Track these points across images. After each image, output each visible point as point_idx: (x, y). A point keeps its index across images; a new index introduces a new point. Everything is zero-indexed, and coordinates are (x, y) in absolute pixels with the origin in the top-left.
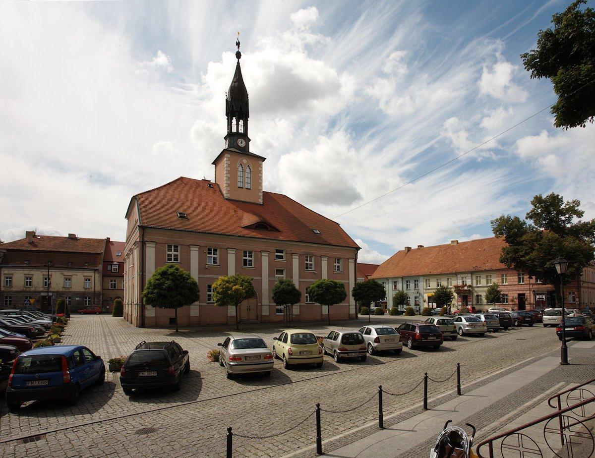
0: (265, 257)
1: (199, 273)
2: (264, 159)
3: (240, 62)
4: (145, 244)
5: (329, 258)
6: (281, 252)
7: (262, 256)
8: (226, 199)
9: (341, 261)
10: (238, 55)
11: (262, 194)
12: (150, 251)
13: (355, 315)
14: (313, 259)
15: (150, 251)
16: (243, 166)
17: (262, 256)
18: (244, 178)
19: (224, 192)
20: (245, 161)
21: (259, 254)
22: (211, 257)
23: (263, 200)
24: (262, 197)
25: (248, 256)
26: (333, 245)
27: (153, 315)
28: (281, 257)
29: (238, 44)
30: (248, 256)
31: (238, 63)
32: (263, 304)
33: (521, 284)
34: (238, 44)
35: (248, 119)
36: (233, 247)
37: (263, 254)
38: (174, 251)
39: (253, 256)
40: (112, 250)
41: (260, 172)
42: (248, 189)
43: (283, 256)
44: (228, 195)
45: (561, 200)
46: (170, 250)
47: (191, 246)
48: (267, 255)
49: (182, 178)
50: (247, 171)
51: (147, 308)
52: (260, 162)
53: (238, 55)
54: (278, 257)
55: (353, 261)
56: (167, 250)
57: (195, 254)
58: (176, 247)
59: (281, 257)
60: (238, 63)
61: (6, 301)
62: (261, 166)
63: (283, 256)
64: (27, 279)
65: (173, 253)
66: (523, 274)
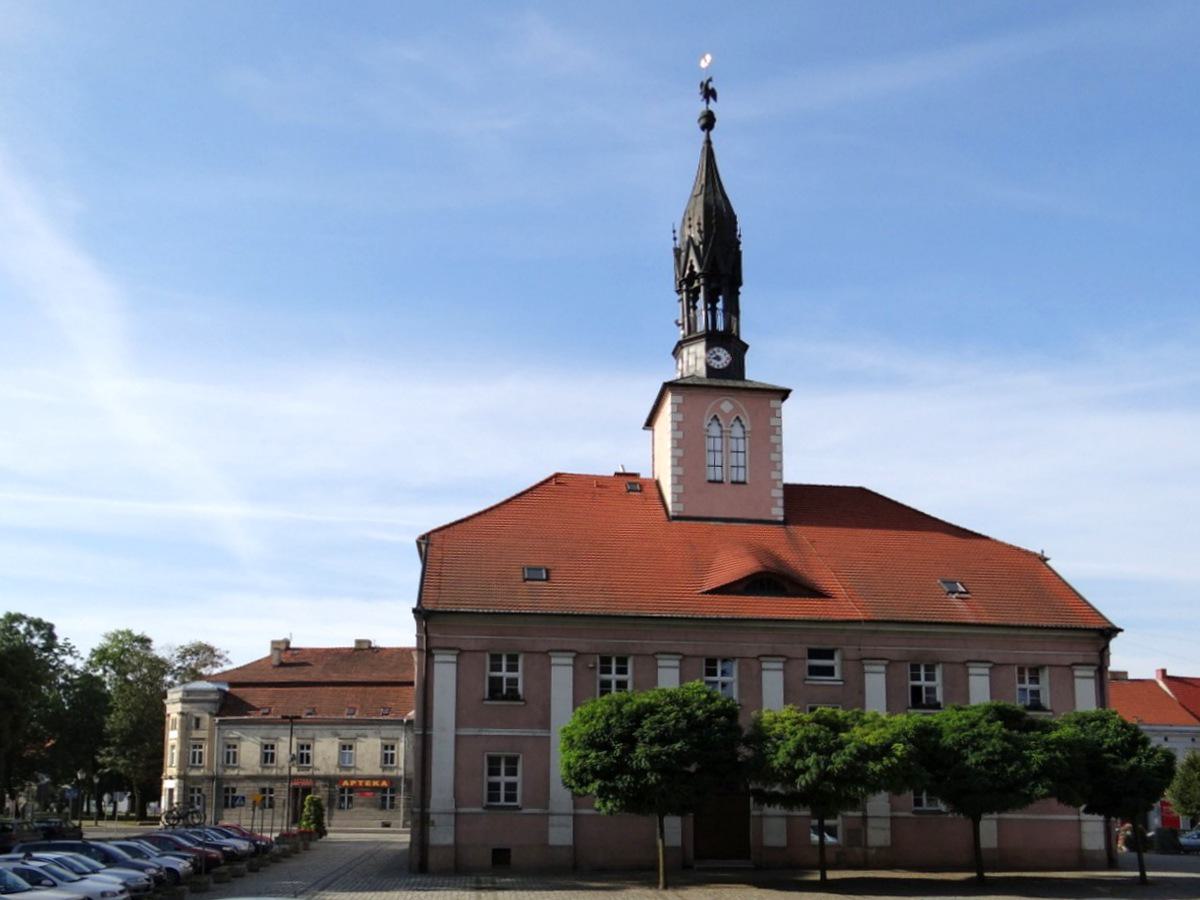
1: (458, 726)
2: (784, 394)
3: (712, 139)
4: (432, 656)
5: (995, 667)
6: (829, 654)
8: (675, 518)
9: (1045, 677)
11: (779, 493)
13: (1105, 855)
14: (938, 672)
16: (721, 422)
18: (727, 456)
19: (668, 499)
20: (727, 406)
21: (754, 663)
22: (716, 682)
23: (786, 508)
24: (781, 502)
25: (504, 667)
27: (450, 840)
28: (829, 671)
29: (709, 94)
30: (504, 667)
31: (709, 142)
32: (870, 813)
33: (502, 808)
35: (741, 289)
36: (673, 650)
37: (765, 665)
38: (1030, 683)
39: (630, 670)
41: (776, 430)
42: (715, 482)
44: (680, 507)
47: (550, 654)
48: (780, 666)
49: (557, 475)
50: (712, 434)
51: (433, 822)
52: (774, 403)
54: (815, 671)
56: (909, 676)
57: (773, 681)
58: (622, 661)
59: (829, 671)
60: (709, 142)
61: (227, 798)
62: (776, 413)
64: (229, 747)
66: (152, 696)
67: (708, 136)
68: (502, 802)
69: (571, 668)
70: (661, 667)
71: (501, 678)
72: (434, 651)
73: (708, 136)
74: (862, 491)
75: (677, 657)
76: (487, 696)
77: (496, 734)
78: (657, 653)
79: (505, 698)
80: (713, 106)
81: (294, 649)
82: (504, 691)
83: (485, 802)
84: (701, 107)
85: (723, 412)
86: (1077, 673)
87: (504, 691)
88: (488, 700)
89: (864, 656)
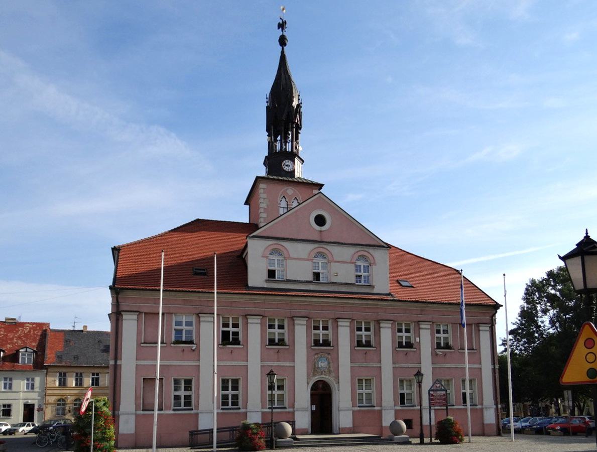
0: (425, 331)
3: (286, 53)
7: (419, 328)
10: (283, 41)
12: (433, 412)
15: (433, 412)
17: (419, 328)
26: (316, 195)
31: (283, 52)
34: (282, 25)
39: (372, 329)
40: (578, 257)
43: (357, 331)
45: (300, 130)
46: (446, 339)
50: (281, 206)
53: (283, 41)
55: (488, 329)
60: (283, 52)
63: (357, 331)
65: (230, 392)
67: (283, 49)
68: (230, 406)
69: (349, 328)
70: (341, 326)
71: (229, 332)
72: (122, 313)
73: (283, 49)
74: (198, 220)
75: (305, 319)
76: (397, 347)
77: (178, 364)
78: (247, 315)
79: (364, 346)
80: (279, 33)
81: (380, 331)
82: (231, 340)
83: (172, 407)
84: (279, 33)
85: (288, 194)
86: (422, 326)
87: (231, 340)
88: (314, 346)
89: (420, 320)
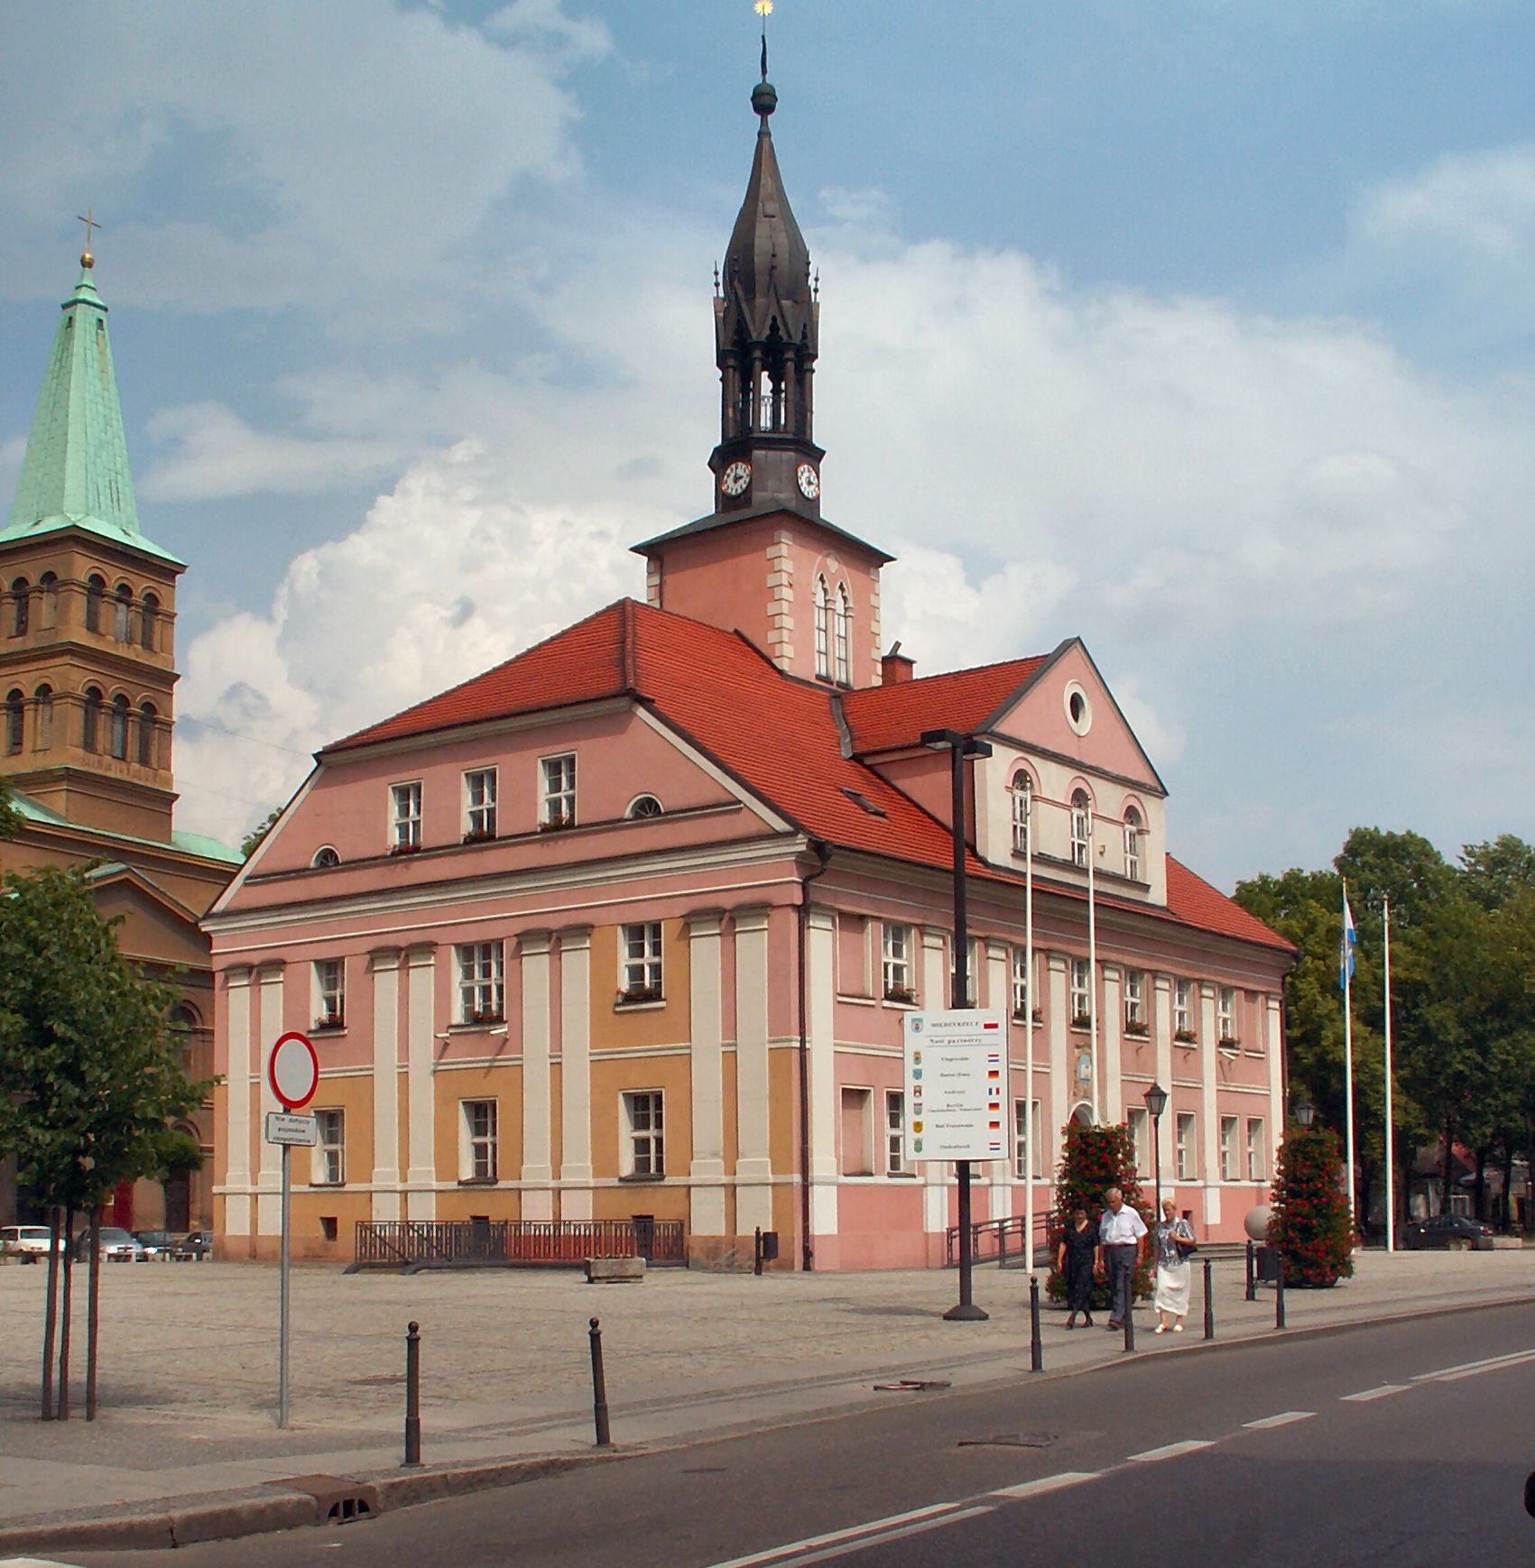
31: (764, 134)
60: (764, 134)
